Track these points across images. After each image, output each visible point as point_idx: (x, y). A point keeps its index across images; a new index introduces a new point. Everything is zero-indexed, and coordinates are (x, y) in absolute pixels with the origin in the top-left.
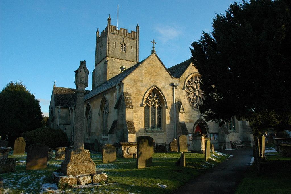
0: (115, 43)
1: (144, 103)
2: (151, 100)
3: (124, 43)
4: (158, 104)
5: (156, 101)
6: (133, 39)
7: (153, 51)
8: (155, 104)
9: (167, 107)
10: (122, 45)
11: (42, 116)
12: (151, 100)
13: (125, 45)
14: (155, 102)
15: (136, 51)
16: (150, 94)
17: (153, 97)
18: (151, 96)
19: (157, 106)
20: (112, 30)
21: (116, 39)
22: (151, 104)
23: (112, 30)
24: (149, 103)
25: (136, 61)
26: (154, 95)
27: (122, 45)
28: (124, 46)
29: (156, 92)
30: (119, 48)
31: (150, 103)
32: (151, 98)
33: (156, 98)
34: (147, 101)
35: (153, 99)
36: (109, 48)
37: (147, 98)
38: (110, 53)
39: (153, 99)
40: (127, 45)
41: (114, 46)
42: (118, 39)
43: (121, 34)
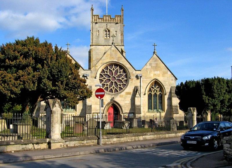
0: (99, 31)
1: (146, 92)
2: (154, 89)
3: (108, 29)
4: (159, 92)
5: (158, 90)
6: (117, 23)
7: (154, 53)
8: (157, 92)
9: (165, 94)
10: (106, 31)
11: (179, 99)
12: (154, 89)
13: (109, 31)
14: (156, 91)
15: (120, 34)
16: (152, 85)
17: (155, 87)
18: (154, 87)
19: (158, 93)
20: (95, 19)
21: (99, 27)
22: (154, 92)
23: (95, 19)
24: (151, 92)
25: (121, 45)
26: (156, 85)
27: (106, 31)
28: (108, 32)
29: (157, 83)
30: (103, 35)
31: (153, 92)
32: (154, 88)
33: (158, 88)
34: (150, 90)
35: (155, 88)
36: (93, 37)
37: (150, 89)
38: (94, 41)
39: (155, 88)
40: (111, 30)
41: (98, 33)
42: (101, 27)
43: (104, 21)
